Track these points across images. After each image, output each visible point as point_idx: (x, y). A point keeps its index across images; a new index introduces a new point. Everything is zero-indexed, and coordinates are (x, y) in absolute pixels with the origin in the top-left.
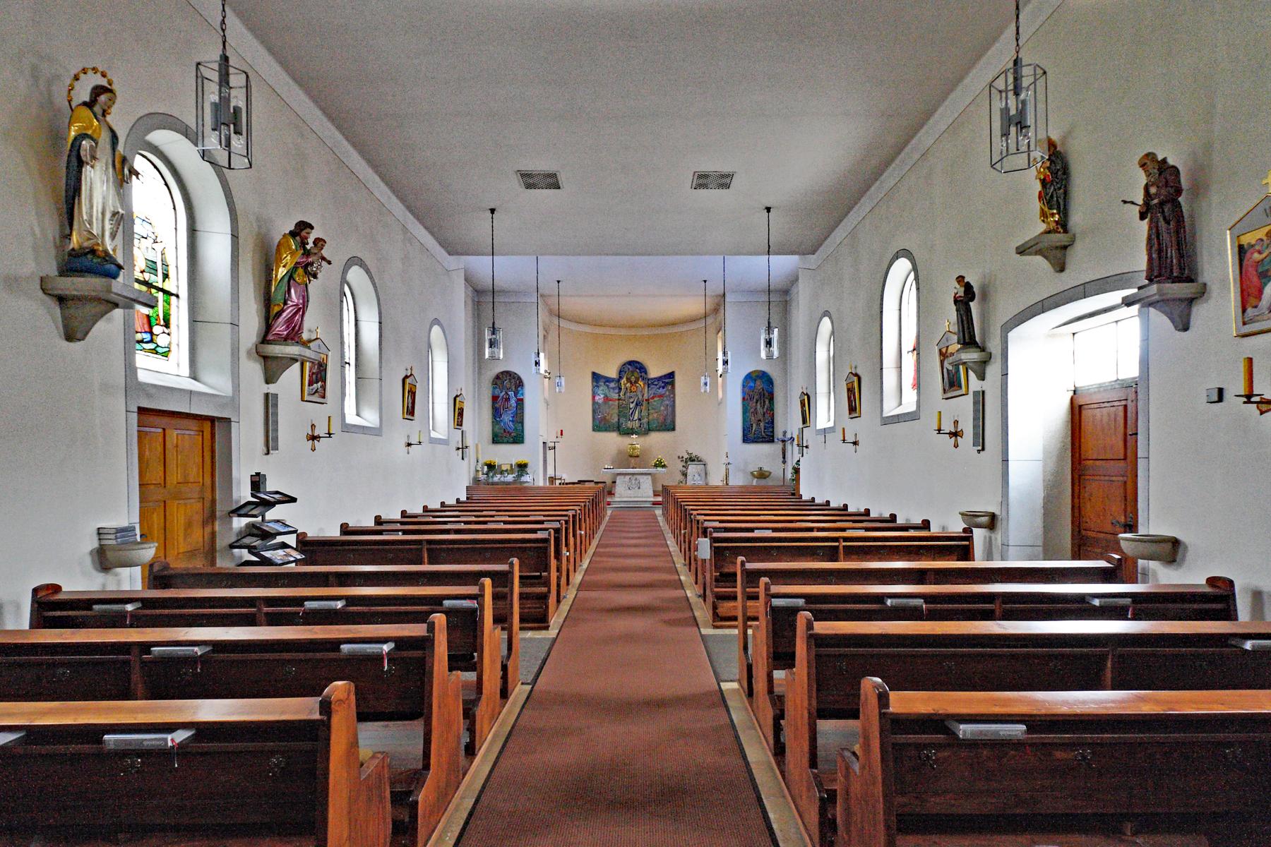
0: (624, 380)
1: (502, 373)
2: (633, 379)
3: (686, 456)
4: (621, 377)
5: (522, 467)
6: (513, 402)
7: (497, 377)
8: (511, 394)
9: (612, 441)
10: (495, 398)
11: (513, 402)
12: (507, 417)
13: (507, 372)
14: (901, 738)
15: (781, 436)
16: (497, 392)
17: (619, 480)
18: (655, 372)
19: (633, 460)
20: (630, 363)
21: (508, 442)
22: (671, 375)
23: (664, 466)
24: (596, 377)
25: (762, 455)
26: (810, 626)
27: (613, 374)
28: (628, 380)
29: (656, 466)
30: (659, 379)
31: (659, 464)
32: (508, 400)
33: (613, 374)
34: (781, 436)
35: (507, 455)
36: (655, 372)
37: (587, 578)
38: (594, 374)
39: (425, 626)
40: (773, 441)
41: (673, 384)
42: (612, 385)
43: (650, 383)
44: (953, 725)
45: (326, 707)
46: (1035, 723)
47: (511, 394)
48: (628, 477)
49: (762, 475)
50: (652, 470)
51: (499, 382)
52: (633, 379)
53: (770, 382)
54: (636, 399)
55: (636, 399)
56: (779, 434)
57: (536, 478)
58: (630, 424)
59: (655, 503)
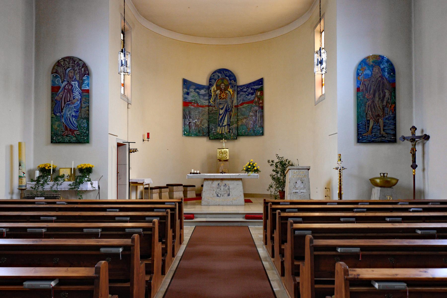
0: (214, 88)
1: (64, 59)
2: (223, 86)
3: (276, 160)
4: (211, 85)
5: (86, 172)
6: (77, 94)
7: (58, 63)
8: (75, 84)
9: (202, 146)
10: (55, 89)
11: (77, 94)
12: (69, 112)
13: (69, 58)
14: (316, 253)
15: (408, 134)
16: (58, 82)
17: (206, 183)
18: (243, 79)
19: (222, 164)
20: (221, 71)
21: (70, 142)
22: (260, 82)
23: (257, 171)
24: (186, 83)
25: (380, 158)
26: (311, 241)
27: (203, 81)
28: (218, 87)
29: (248, 170)
30: (248, 86)
31: (251, 169)
32: (71, 91)
33: (203, 81)
34: (408, 134)
35: (68, 157)
36: (243, 79)
37: (185, 263)
38: (185, 82)
39: (93, 269)
40: (393, 141)
41: (261, 90)
42: (202, 92)
43: (240, 89)
44: (373, 283)
45: (98, 271)
46: (410, 282)
47: (75, 84)
48: (216, 183)
49: (387, 183)
50: (243, 175)
51: (60, 70)
52: (223, 86)
53: (392, 70)
54: (225, 106)
55: (225, 106)
56: (404, 130)
57: (107, 187)
58: (219, 130)
59: (249, 216)
